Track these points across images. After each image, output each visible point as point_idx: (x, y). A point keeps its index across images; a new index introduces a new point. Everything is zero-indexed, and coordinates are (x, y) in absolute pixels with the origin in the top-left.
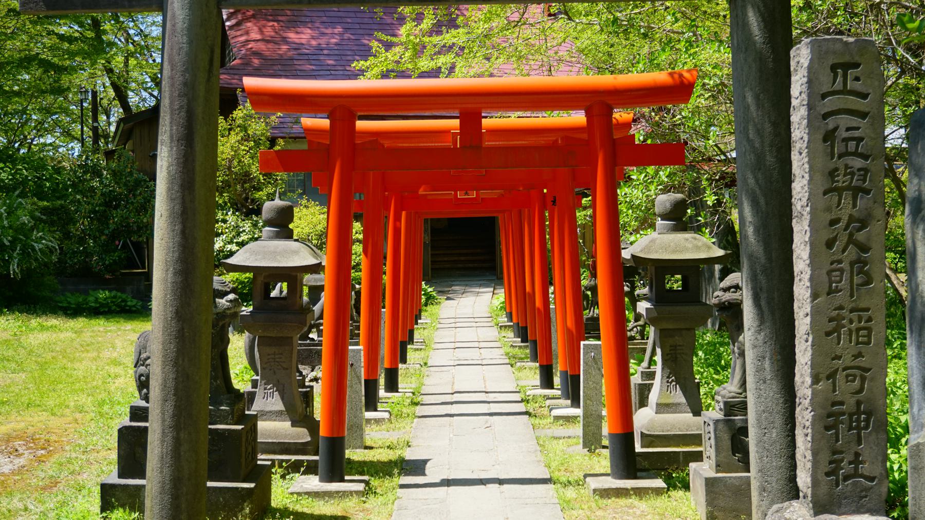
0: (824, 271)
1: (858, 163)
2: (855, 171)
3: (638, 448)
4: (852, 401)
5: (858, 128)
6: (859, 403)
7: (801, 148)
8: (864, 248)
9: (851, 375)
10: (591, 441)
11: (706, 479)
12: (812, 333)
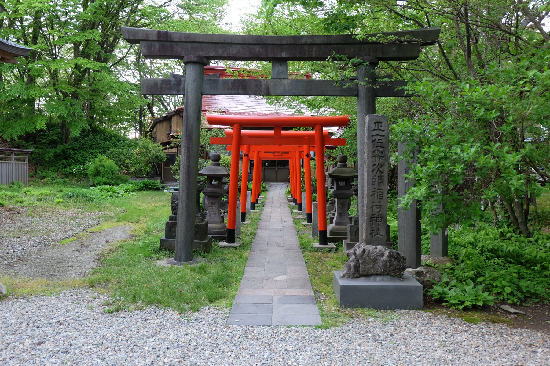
1: (381, 149)
3: (328, 236)
4: (377, 214)
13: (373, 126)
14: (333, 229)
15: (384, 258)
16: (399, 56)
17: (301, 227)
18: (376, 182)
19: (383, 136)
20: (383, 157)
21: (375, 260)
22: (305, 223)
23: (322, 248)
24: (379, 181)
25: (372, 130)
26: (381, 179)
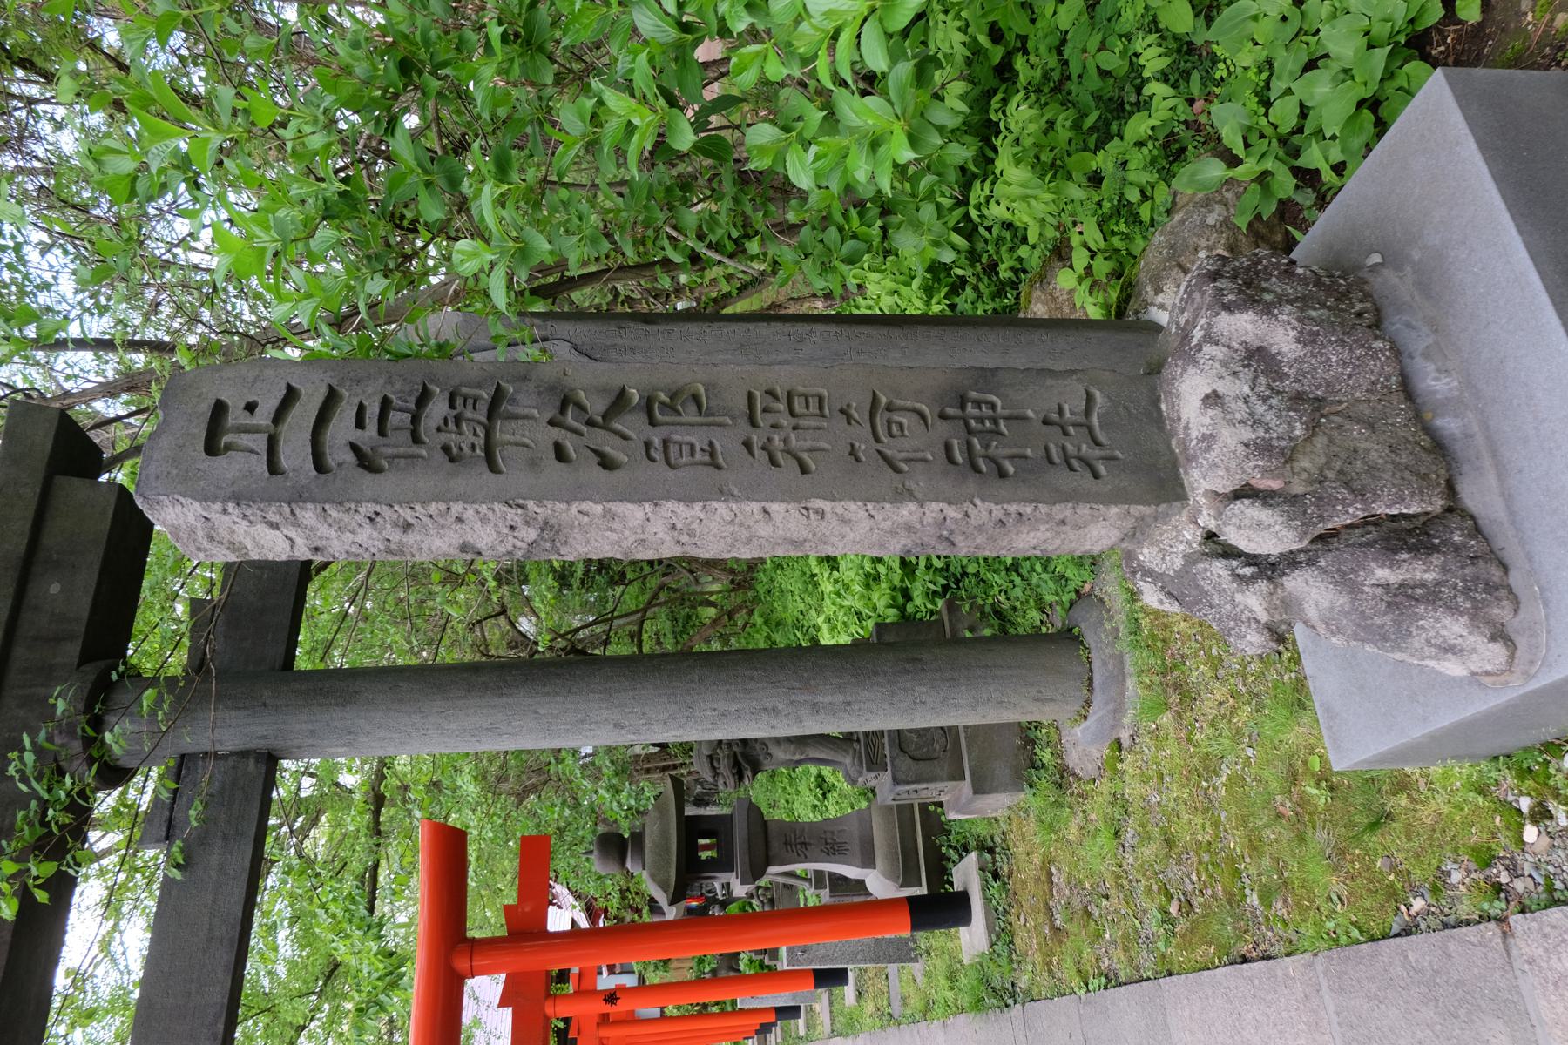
0: (671, 473)
1: (438, 409)
2: (455, 412)
3: (923, 890)
4: (942, 429)
5: (361, 409)
6: (943, 416)
7: (395, 524)
8: (620, 401)
9: (889, 429)
10: (904, 953)
11: (975, 793)
12: (807, 499)
13: (244, 464)
14: (891, 876)
15: (1283, 338)
16: (97, 567)
17: (870, 1007)
18: (698, 439)
19: (332, 398)
20: (498, 396)
21: (1312, 406)
22: (849, 991)
23: (992, 913)
24: (690, 415)
25: (273, 467)
26: (670, 408)
